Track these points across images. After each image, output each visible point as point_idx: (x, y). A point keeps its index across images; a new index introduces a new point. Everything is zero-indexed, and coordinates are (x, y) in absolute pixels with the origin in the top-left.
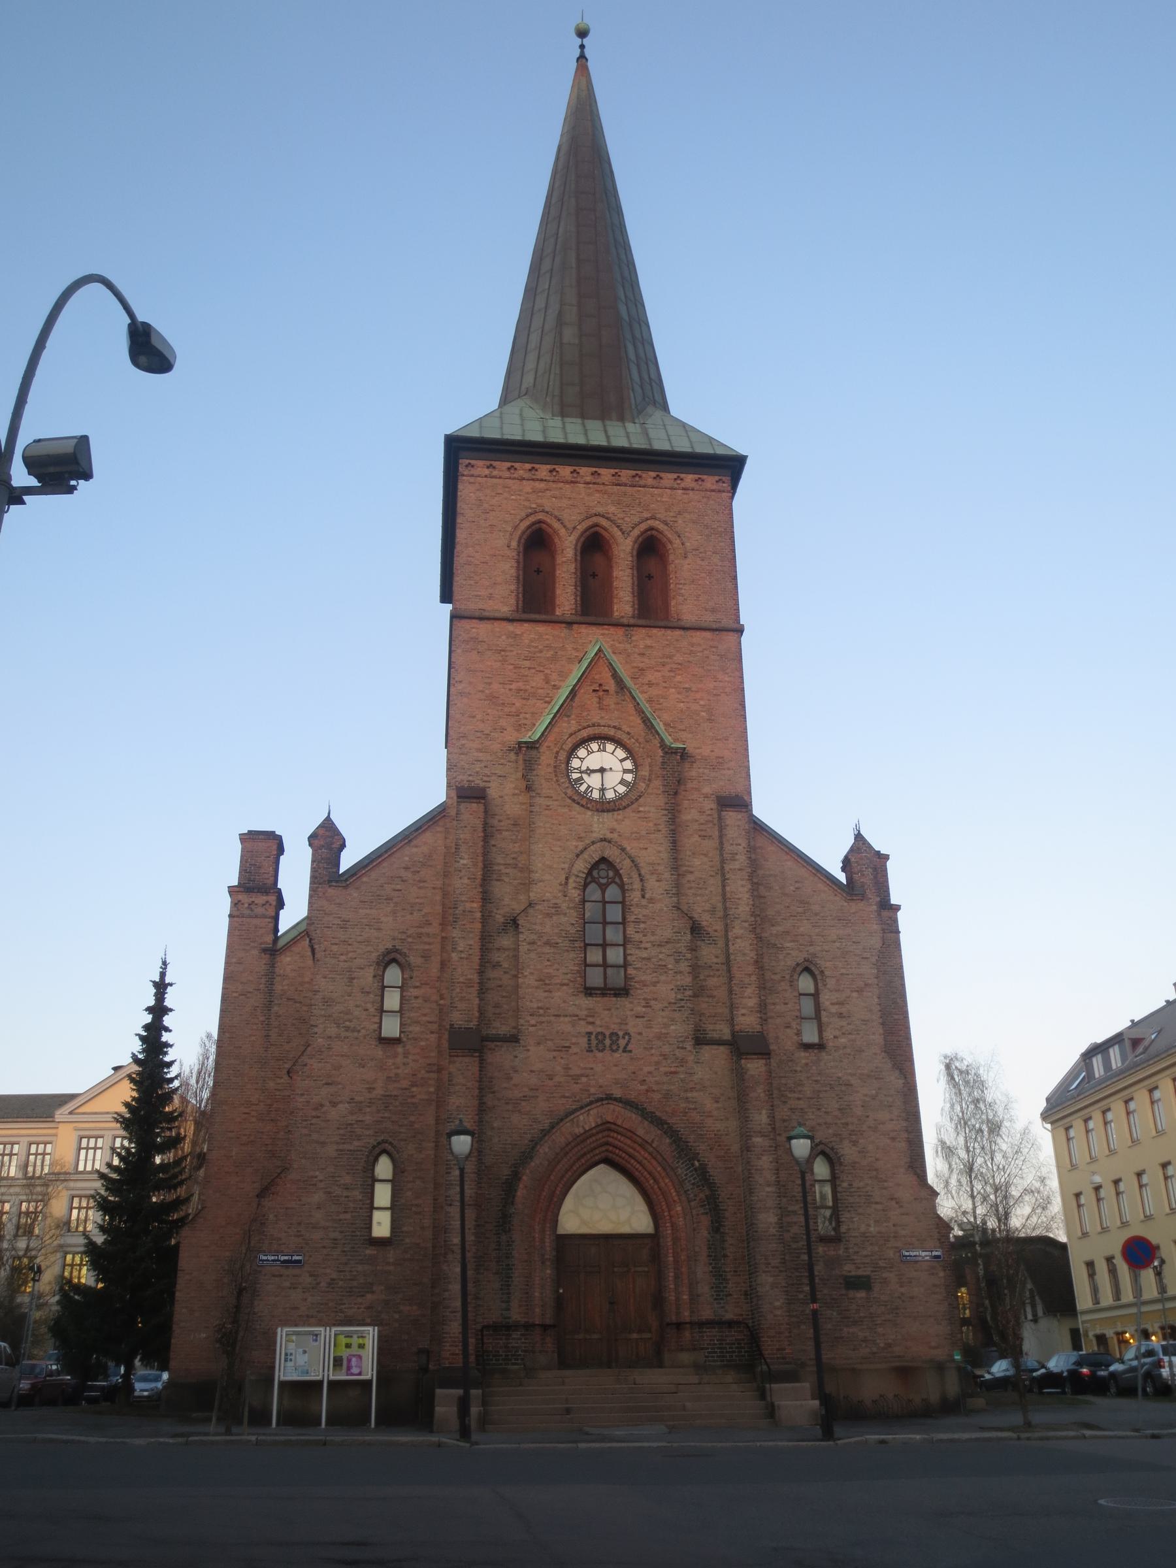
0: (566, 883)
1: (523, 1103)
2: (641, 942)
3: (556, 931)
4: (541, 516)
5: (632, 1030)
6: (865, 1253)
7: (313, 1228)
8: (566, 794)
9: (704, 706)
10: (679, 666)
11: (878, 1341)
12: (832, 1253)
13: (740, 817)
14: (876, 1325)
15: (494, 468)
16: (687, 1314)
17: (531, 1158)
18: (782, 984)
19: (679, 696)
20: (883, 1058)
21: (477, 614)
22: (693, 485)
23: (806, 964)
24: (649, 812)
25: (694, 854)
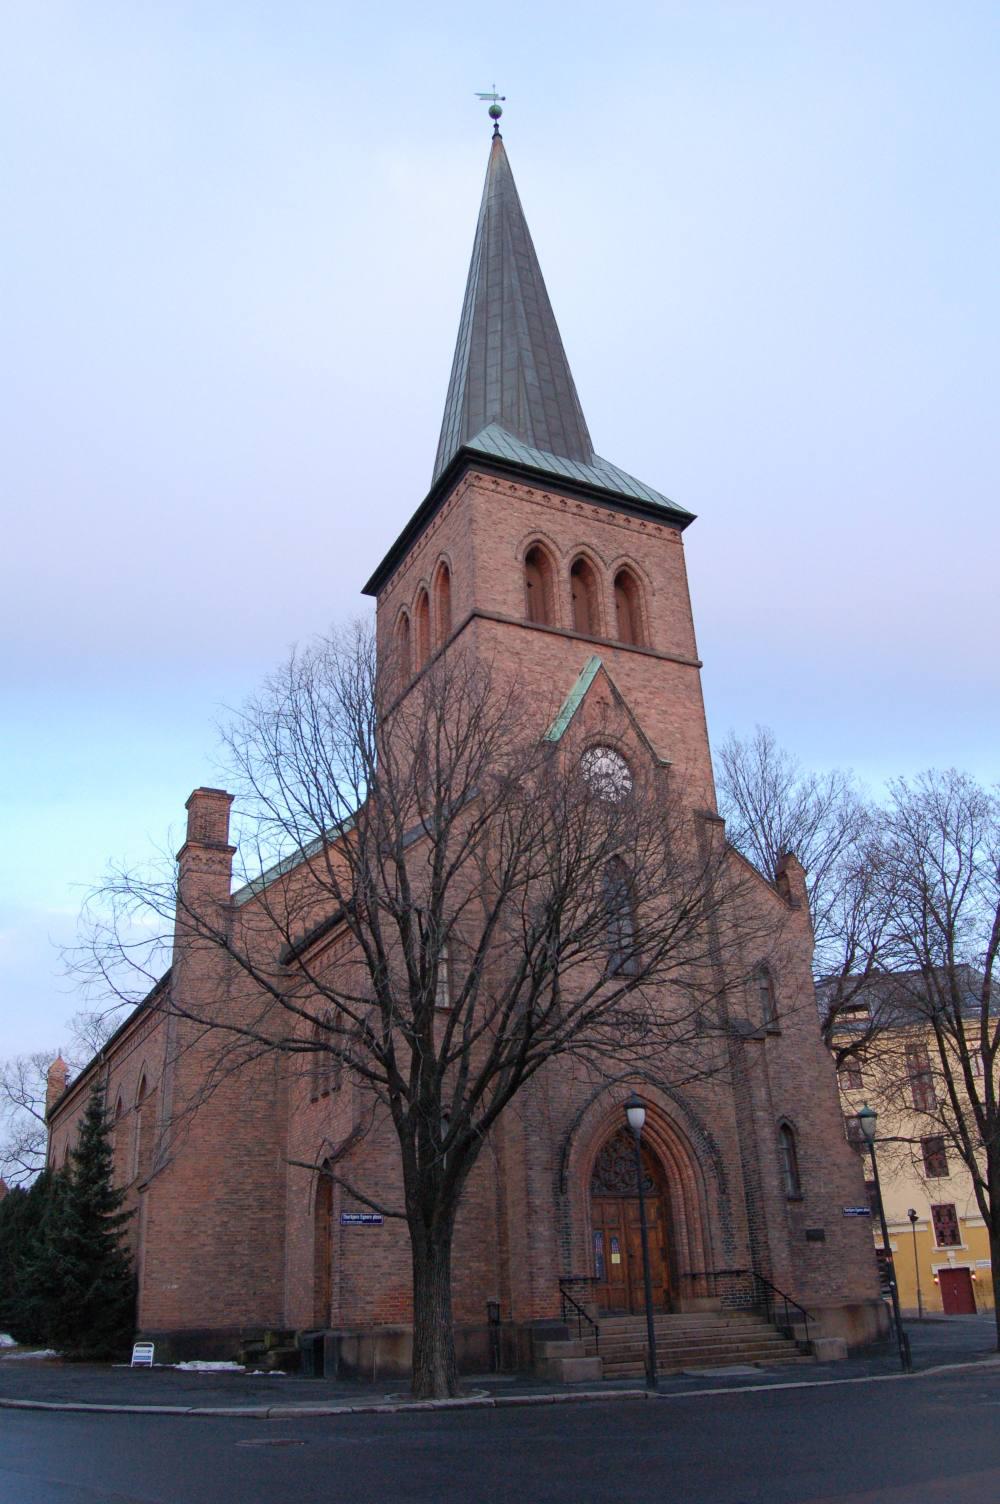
4: (539, 536)
6: (818, 1210)
7: (389, 1188)
9: (677, 728)
12: (797, 1210)
15: (498, 484)
16: (702, 1265)
21: (496, 616)
22: (654, 532)
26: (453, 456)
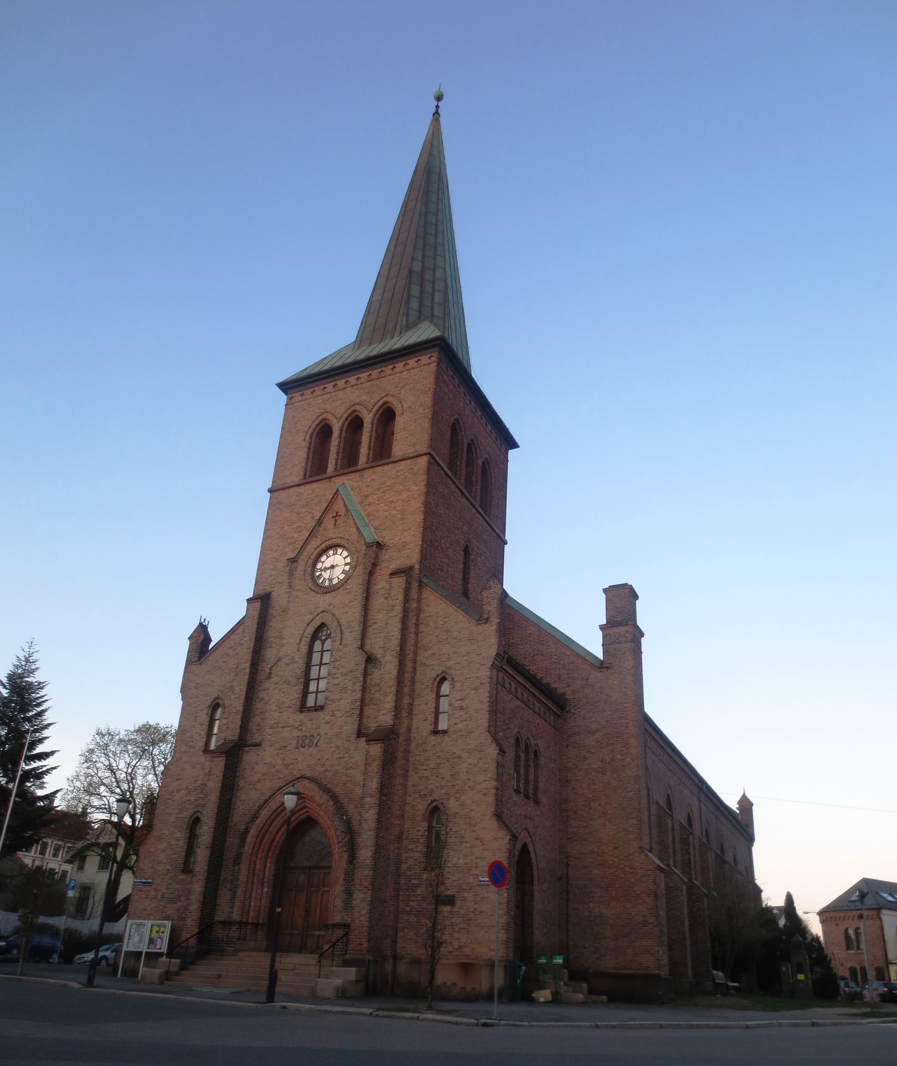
0: (300, 643)
1: (258, 784)
2: (335, 674)
3: (291, 673)
4: (324, 416)
5: (322, 732)
6: (454, 878)
8: (308, 586)
10: (388, 488)
11: (454, 944)
13: (401, 580)
14: (454, 931)
17: (257, 818)
18: (426, 690)
19: (386, 508)
20: (486, 736)
21: (281, 487)
23: (443, 674)
24: (352, 588)
25: (379, 610)
26: (420, 339)
